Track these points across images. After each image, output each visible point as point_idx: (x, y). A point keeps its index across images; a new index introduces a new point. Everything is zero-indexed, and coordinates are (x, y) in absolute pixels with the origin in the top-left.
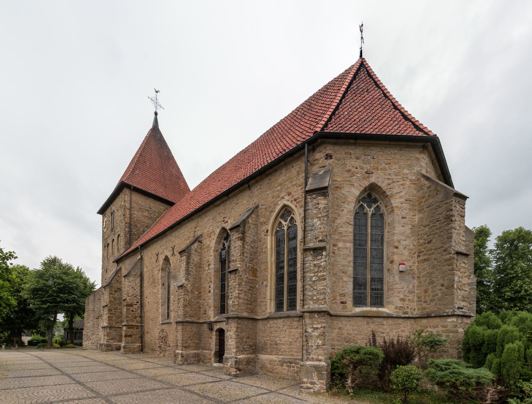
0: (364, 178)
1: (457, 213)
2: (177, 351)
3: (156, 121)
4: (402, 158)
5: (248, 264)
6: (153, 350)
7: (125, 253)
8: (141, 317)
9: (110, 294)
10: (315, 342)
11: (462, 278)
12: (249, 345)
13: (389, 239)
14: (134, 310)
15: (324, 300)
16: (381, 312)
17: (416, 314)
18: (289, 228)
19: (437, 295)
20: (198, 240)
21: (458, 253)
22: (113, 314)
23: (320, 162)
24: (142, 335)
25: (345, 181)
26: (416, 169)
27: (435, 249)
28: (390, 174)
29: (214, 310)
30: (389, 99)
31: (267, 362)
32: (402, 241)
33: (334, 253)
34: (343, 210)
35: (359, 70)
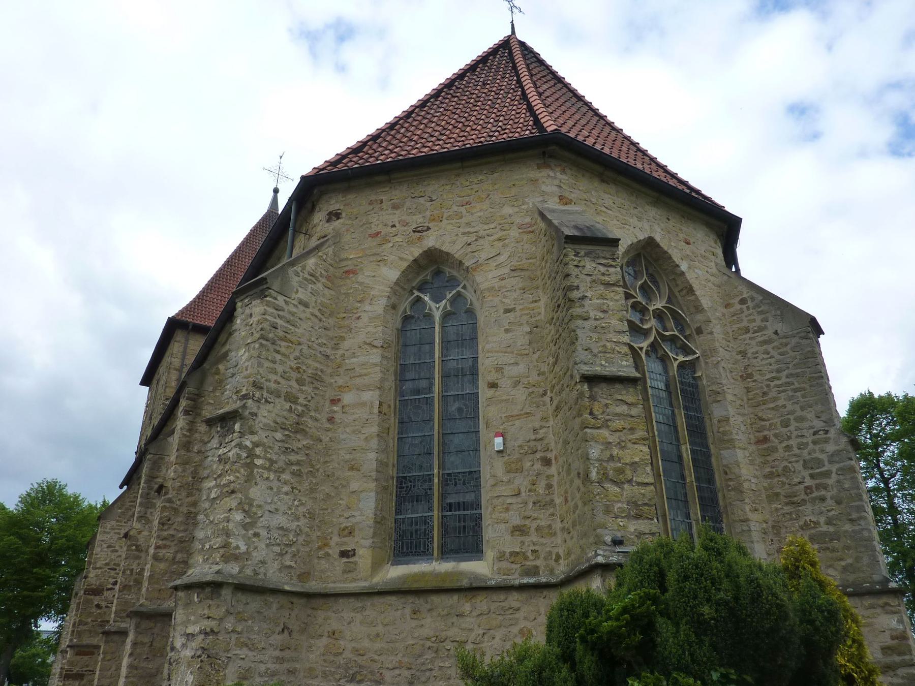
0: (410, 242)
1: (589, 279)
4: (496, 187)
14: (103, 604)
16: (462, 574)
21: (592, 380)
23: (319, 228)
26: (533, 201)
28: (468, 224)
33: (331, 420)
34: (359, 318)
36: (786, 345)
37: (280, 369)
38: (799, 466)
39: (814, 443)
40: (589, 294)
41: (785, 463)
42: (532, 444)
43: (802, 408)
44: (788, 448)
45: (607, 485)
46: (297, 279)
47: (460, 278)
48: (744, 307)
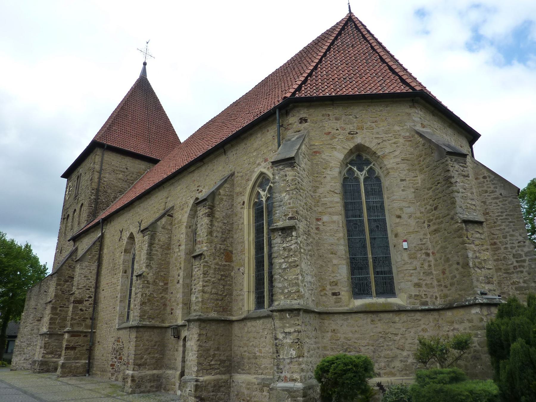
0: (348, 139)
1: (457, 173)
2: (127, 372)
3: (144, 71)
4: (390, 115)
5: (218, 246)
6: (104, 371)
7: (85, 229)
8: (93, 319)
9: (58, 285)
10: (288, 353)
11: (480, 253)
12: (220, 360)
13: (390, 207)
14: (84, 309)
15: (297, 294)
16: (390, 304)
17: (440, 304)
18: (268, 199)
19: (455, 277)
20: (168, 213)
21: (466, 222)
22: (57, 314)
23: (294, 126)
24: (91, 347)
25: (324, 144)
26: (409, 124)
27: (443, 217)
28: (378, 133)
29: (183, 309)
30: (377, 53)
31: (244, 385)
32: (405, 209)
33: (317, 229)
34: (325, 177)
35: (346, 24)
36: (506, 201)
38: (511, 257)
39: (518, 247)
41: (505, 255)
42: (420, 246)
43: (513, 231)
44: (506, 248)
45: (476, 269)
47: (371, 160)
48: (485, 180)
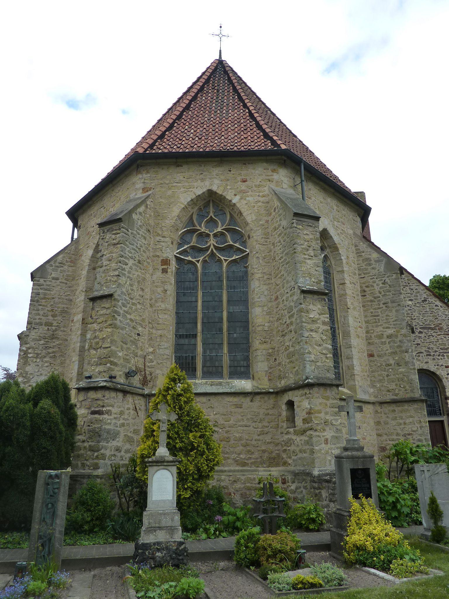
1: (107, 244)
37: (41, 313)
40: (105, 253)
46: (51, 268)
